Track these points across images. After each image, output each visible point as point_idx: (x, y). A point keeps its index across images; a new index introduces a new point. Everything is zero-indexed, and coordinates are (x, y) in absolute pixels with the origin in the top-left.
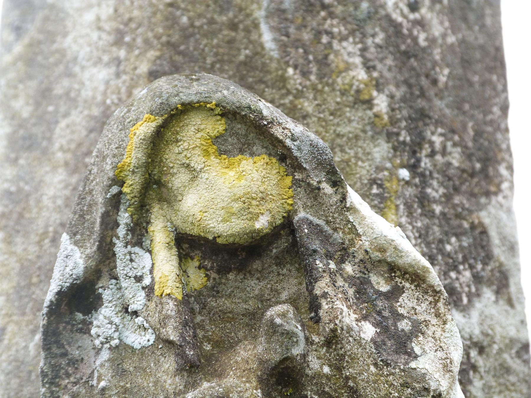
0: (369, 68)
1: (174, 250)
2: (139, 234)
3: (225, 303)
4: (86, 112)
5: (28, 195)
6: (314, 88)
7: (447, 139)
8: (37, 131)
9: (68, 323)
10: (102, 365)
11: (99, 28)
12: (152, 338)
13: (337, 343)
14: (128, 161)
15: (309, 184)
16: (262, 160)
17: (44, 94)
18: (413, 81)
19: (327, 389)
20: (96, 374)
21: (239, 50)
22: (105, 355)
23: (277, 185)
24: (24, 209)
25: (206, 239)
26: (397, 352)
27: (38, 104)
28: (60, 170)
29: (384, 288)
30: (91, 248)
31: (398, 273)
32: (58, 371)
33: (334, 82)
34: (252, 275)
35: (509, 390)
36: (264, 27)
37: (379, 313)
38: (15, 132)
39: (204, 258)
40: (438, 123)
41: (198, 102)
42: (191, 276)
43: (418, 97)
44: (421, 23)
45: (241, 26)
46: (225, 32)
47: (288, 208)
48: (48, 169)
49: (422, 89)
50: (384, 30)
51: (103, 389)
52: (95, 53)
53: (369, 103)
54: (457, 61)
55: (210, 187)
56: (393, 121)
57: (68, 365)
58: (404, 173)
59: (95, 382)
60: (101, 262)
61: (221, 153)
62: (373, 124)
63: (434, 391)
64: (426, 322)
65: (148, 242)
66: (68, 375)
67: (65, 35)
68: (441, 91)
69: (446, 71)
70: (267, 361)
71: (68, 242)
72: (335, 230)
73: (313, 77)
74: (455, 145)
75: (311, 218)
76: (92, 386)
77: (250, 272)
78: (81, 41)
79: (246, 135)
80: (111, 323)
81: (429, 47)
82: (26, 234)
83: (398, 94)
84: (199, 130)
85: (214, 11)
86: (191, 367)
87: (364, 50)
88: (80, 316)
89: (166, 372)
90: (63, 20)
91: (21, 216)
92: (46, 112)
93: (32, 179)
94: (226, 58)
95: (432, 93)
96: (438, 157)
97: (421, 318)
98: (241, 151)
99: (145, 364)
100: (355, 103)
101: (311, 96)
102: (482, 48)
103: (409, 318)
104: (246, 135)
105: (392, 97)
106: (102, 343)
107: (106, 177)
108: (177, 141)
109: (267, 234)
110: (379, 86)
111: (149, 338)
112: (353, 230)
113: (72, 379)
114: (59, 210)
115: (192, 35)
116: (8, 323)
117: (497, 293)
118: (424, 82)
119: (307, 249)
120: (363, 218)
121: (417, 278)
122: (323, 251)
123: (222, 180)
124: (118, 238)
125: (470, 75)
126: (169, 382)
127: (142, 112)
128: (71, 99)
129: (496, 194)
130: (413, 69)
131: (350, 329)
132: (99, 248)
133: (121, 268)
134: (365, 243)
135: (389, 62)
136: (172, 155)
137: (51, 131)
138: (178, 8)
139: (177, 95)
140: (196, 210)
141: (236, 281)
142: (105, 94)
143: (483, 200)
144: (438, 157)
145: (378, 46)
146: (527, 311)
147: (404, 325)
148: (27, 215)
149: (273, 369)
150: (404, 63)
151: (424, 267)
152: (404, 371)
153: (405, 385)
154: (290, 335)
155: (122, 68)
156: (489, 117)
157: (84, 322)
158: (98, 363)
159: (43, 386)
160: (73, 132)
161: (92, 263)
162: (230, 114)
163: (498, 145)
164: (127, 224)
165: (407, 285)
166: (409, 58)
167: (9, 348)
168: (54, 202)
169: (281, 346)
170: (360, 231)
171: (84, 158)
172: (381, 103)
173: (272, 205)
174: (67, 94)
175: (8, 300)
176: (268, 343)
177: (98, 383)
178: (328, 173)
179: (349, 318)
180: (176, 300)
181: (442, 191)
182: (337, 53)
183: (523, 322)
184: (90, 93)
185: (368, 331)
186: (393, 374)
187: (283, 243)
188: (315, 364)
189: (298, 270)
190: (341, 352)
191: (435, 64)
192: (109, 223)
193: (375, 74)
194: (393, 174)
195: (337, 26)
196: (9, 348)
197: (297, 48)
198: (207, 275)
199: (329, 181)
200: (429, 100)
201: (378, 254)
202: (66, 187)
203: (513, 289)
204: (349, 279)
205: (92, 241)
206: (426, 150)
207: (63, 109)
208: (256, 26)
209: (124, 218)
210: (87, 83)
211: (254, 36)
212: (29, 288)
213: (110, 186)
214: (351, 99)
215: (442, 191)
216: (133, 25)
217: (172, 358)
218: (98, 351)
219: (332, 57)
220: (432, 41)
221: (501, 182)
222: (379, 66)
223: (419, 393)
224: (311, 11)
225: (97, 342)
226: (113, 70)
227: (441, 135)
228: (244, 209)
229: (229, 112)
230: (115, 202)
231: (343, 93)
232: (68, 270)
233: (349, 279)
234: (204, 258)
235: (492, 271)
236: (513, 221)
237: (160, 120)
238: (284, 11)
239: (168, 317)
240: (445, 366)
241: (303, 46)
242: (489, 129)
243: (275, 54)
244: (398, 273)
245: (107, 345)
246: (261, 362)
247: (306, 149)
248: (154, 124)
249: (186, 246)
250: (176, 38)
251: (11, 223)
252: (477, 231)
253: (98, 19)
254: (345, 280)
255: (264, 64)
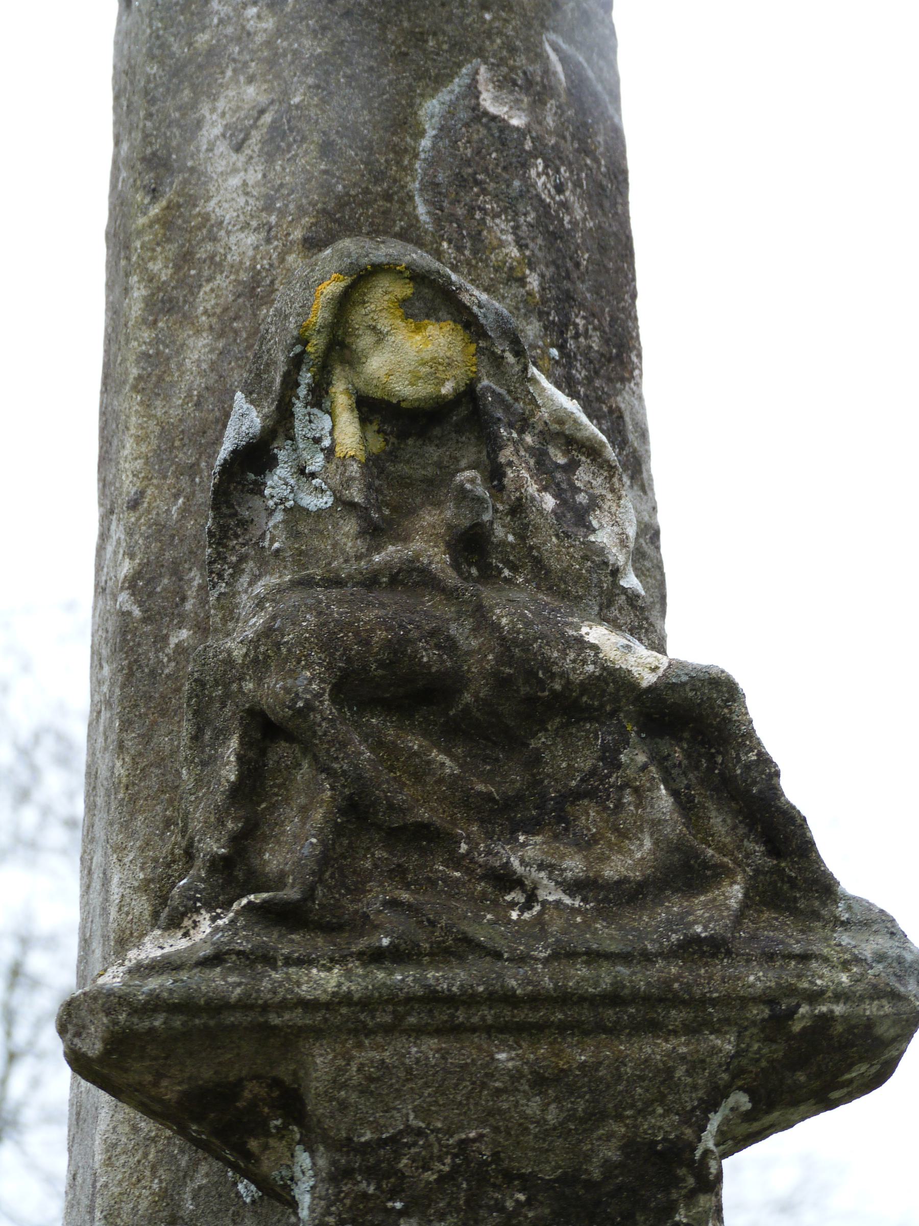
0: (521, 246)
1: (356, 412)
2: (319, 397)
3: (403, 468)
4: (232, 277)
5: (168, 359)
6: (468, 263)
7: (589, 323)
8: (179, 294)
9: (239, 483)
10: (275, 527)
11: (247, 194)
12: (330, 501)
13: (521, 512)
14: (314, 320)
15: (493, 353)
16: (448, 326)
17: (185, 258)
18: (560, 262)
19: (511, 558)
20: (268, 536)
21: (395, 222)
22: (279, 516)
23: (462, 351)
24: (165, 372)
25: (389, 403)
26: (576, 525)
27: (178, 268)
28: (205, 335)
29: (561, 460)
30: (269, 407)
31: (575, 446)
32: (227, 531)
33: (488, 258)
34: (431, 441)
35: (645, 575)
36: (418, 200)
37: (558, 485)
38: (153, 294)
39: (383, 422)
40: (581, 306)
41: (388, 264)
42: (370, 440)
43: (564, 278)
44: (564, 205)
45: (396, 198)
46: (380, 203)
47: (471, 375)
48: (191, 333)
49: (567, 271)
50: (535, 209)
51: (278, 551)
52: (242, 218)
53: (522, 281)
54: (596, 246)
55: (396, 350)
56: (544, 301)
57: (237, 525)
58: (554, 352)
59: (266, 544)
60: (278, 422)
61: (407, 316)
62: (526, 302)
63: (613, 565)
64: (603, 497)
65: (329, 403)
66: (237, 536)
67: (209, 199)
68: (582, 274)
69: (586, 256)
70: (456, 526)
71: (244, 401)
72: (516, 399)
73: (467, 253)
74: (595, 329)
75: (494, 387)
76: (263, 547)
77: (429, 439)
78: (226, 205)
79: (433, 301)
80: (286, 484)
81: (572, 229)
82: (167, 398)
83: (548, 275)
84: (386, 293)
85: (369, 181)
86: (375, 530)
87: (516, 228)
88: (252, 476)
89: (346, 535)
90: (205, 183)
91: (160, 379)
92: (187, 276)
93: (174, 342)
94: (381, 228)
95: (575, 275)
96: (582, 340)
97: (597, 492)
98: (428, 316)
99: (321, 526)
100: (508, 280)
101: (466, 271)
102: (615, 234)
103: (586, 492)
104: (433, 301)
105: (542, 276)
106: (276, 504)
107: (289, 336)
108: (364, 302)
109: (451, 401)
110: (531, 266)
111: (325, 501)
112: (533, 401)
113: (240, 540)
114: (202, 374)
115: (348, 203)
116: (147, 486)
117: (632, 478)
118: (569, 264)
119: (492, 417)
120: (543, 389)
121: (593, 451)
122: (506, 420)
123: (409, 344)
124: (298, 398)
125: (606, 262)
126: (350, 544)
127: (328, 272)
128: (216, 263)
129: (629, 380)
130: (559, 250)
131: (533, 499)
132: (278, 407)
133: (299, 428)
134: (544, 414)
135: (540, 241)
136: (358, 317)
137: (194, 295)
138: (333, 176)
139: (367, 256)
140: (382, 373)
141: (415, 446)
142: (254, 259)
143: (618, 385)
144: (582, 340)
145: (530, 225)
146: (657, 498)
147: (582, 498)
148: (168, 379)
149: (462, 534)
150: (552, 244)
151: (601, 441)
152: (583, 543)
153: (586, 558)
154: (480, 500)
155: (272, 233)
156: (623, 304)
157: (255, 482)
158: (271, 524)
159: (210, 546)
160: (217, 296)
161: (269, 422)
162: (419, 278)
163: (629, 333)
164: (308, 384)
165: (583, 459)
166: (556, 239)
167: (148, 511)
168: (198, 366)
169: (471, 512)
170: (539, 402)
171: (231, 323)
172: (534, 282)
173: (456, 372)
174: (212, 258)
175: (146, 463)
176: (457, 508)
177: (271, 544)
178: (511, 343)
179: (532, 488)
180: (360, 462)
181: (584, 373)
182: (490, 230)
183: (654, 509)
184: (237, 258)
185: (549, 502)
186: (573, 546)
187: (463, 411)
188: (499, 532)
189: (478, 438)
190: (525, 521)
191: (578, 247)
192: (290, 383)
193: (528, 253)
194: (545, 352)
195: (490, 202)
196: (148, 511)
197: (451, 222)
198: (386, 440)
199: (511, 351)
200: (574, 283)
201: (557, 426)
202: (212, 351)
203: (645, 475)
204: (528, 449)
205: (269, 400)
206: (571, 332)
207: (206, 273)
208: (411, 198)
209: (306, 377)
210: (234, 248)
211: (409, 209)
212: (171, 452)
213: (294, 345)
214: (504, 275)
215: (584, 373)
216: (285, 192)
217: (353, 520)
218: (271, 512)
219: (485, 233)
220: (574, 223)
221: (634, 369)
222: (531, 245)
223: (598, 566)
224: (465, 187)
225: (271, 503)
226: (263, 235)
227: (583, 317)
228: (431, 374)
229: (418, 275)
230: (297, 363)
231: (497, 269)
232: (244, 428)
233: (528, 449)
234: (383, 422)
235: (627, 456)
236: (643, 408)
237: (348, 280)
238: (438, 185)
239: (352, 479)
240: (622, 541)
241: (457, 221)
242: (622, 316)
243: (430, 227)
244: (575, 446)
245: (282, 507)
246: (450, 527)
247: (492, 317)
248: (343, 284)
249: (365, 409)
250: (331, 206)
251: (150, 385)
252: (615, 416)
253: (245, 184)
254: (526, 451)
255: (419, 236)
